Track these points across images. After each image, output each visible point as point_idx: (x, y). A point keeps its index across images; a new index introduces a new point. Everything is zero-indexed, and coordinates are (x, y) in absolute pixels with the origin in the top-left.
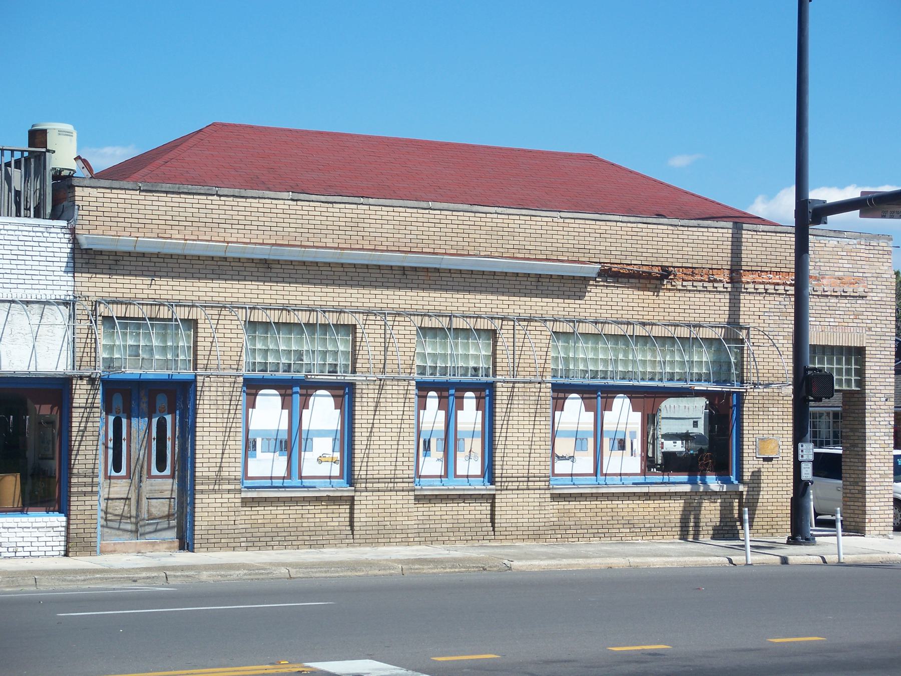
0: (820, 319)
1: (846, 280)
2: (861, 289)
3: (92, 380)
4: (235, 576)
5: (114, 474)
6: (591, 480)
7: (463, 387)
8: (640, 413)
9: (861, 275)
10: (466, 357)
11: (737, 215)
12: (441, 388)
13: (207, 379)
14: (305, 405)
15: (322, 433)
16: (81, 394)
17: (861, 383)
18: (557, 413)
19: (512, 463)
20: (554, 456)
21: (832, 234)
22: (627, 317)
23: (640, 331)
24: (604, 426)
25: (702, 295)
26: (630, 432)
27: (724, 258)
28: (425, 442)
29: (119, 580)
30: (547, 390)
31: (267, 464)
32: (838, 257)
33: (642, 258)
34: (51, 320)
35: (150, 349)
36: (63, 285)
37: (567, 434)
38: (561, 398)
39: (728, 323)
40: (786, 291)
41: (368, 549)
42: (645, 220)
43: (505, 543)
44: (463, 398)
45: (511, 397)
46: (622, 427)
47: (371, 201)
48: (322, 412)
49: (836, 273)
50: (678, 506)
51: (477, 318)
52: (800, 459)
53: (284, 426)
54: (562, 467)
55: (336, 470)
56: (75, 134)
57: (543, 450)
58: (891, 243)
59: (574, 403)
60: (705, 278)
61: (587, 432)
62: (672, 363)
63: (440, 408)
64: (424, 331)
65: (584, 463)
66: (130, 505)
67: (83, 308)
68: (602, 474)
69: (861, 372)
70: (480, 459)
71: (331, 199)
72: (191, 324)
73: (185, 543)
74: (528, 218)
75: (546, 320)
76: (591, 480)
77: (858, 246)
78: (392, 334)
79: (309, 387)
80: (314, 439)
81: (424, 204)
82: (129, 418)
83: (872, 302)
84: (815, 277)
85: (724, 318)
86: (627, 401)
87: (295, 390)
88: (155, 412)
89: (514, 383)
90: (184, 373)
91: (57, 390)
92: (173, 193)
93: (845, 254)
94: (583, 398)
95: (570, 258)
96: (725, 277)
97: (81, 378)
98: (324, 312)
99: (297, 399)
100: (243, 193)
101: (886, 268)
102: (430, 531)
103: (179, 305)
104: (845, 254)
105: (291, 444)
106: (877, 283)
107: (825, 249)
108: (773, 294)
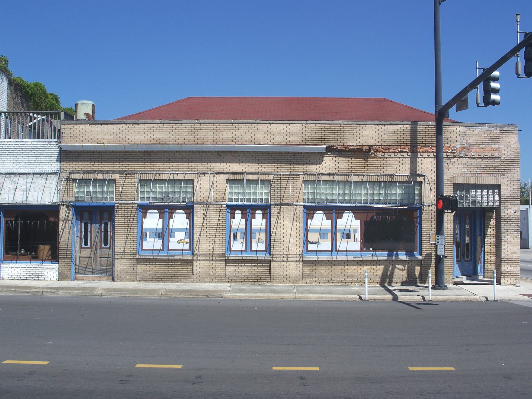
1: (487, 149)
2: (497, 154)
3: (68, 206)
4: (75, 294)
5: (104, 247)
7: (254, 208)
10: (255, 193)
14: (171, 217)
16: (63, 213)
18: (309, 221)
21: (477, 125)
22: (348, 171)
23: (355, 178)
25: (394, 159)
26: (354, 230)
27: (407, 140)
28: (234, 234)
29: (21, 292)
30: (300, 209)
31: (152, 244)
34: (51, 181)
36: (56, 167)
37: (315, 231)
38: (311, 214)
39: (410, 173)
41: (197, 284)
42: (357, 123)
43: (262, 283)
44: (255, 214)
45: (279, 212)
46: (348, 227)
47: (201, 121)
48: (179, 220)
49: (481, 146)
50: (380, 269)
53: (160, 226)
54: (311, 247)
55: (187, 247)
57: (298, 239)
58: (517, 129)
60: (396, 151)
62: (379, 194)
63: (242, 218)
65: (326, 245)
66: (91, 260)
67: (65, 175)
68: (336, 251)
70: (265, 242)
71: (180, 122)
72: (112, 181)
73: (113, 280)
78: (213, 184)
79: (173, 209)
81: (230, 121)
82: (91, 224)
85: (408, 171)
86: (351, 214)
88: (83, 220)
90: (109, 202)
97: (64, 205)
98: (177, 174)
99: (167, 214)
100: (137, 122)
102: (235, 276)
105: (165, 234)
107: (473, 133)
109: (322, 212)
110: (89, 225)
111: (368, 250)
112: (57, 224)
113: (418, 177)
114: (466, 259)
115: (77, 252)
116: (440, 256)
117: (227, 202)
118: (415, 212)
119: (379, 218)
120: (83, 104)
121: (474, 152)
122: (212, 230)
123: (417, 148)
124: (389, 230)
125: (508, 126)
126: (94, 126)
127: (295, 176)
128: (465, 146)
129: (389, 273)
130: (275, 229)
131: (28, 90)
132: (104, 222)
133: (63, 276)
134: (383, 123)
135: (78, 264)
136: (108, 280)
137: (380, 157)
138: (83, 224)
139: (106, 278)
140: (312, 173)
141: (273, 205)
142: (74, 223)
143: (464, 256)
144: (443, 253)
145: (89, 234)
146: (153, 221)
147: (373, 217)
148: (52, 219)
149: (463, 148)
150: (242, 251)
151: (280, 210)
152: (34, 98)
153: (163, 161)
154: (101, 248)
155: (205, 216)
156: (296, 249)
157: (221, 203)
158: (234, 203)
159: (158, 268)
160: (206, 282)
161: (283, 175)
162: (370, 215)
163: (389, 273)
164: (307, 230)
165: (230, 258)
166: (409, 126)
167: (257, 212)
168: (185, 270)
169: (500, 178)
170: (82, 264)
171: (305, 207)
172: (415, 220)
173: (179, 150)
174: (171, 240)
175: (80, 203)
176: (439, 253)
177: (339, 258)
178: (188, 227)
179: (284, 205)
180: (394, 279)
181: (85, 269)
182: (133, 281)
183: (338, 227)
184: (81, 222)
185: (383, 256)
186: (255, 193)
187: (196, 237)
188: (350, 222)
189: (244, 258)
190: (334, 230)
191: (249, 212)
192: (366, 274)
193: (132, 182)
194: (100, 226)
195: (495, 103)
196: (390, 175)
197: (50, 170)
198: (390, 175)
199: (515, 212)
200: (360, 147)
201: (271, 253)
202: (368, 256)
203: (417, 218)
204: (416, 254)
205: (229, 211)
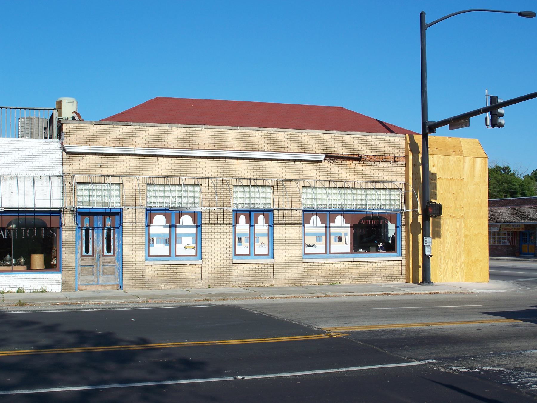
15: (263, 235)
16: (68, 218)
20: (305, 245)
28: (239, 239)
52: (425, 245)
56: (75, 102)
59: (315, 220)
65: (321, 248)
67: (68, 179)
70: (267, 247)
103: (320, 181)
116: (428, 256)
145: (91, 241)
154: (103, 255)
158: (240, 207)
176: (427, 253)
188: (341, 226)
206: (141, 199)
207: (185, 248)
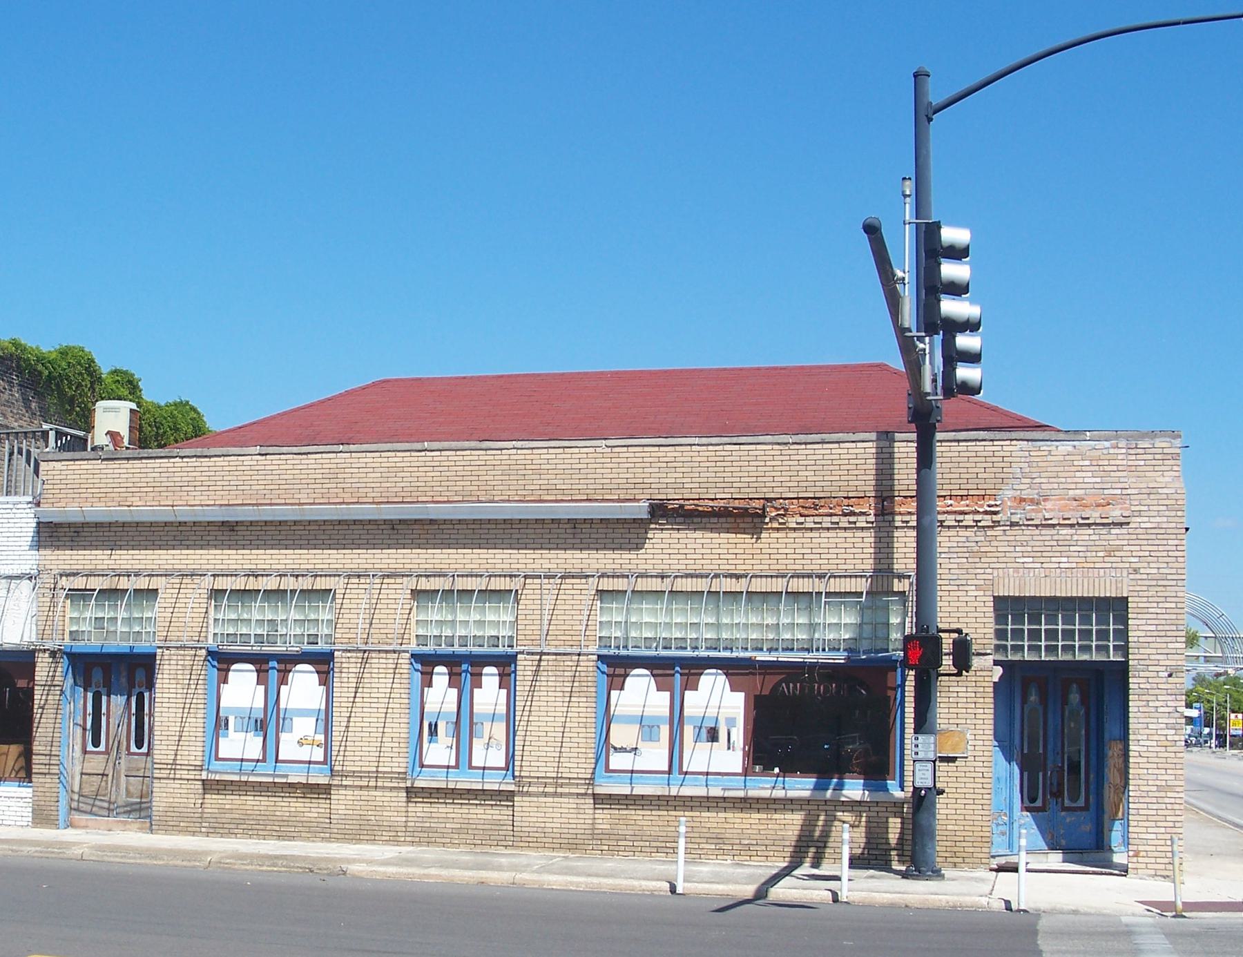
0: (1042, 560)
3: (53, 654)
4: (25, 853)
6: (738, 781)
8: (742, 694)
9: (1119, 492)
11: (997, 421)
12: (453, 662)
13: (167, 652)
14: (283, 681)
17: (1124, 649)
18: (614, 694)
19: (538, 754)
22: (709, 566)
24: (426, 706)
25: (831, 534)
26: (727, 719)
27: (866, 482)
28: (430, 725)
31: (240, 744)
32: (1073, 469)
33: (732, 490)
35: (1052, 634)
36: (28, 560)
37: (628, 719)
39: (875, 570)
40: (977, 521)
42: (735, 440)
44: (481, 674)
45: (536, 672)
46: (712, 712)
47: (352, 448)
48: (303, 687)
49: (1071, 492)
50: (793, 822)
51: (490, 576)
53: (259, 703)
54: (617, 761)
55: (319, 755)
57: (583, 739)
58: (1178, 442)
59: (639, 684)
60: (837, 511)
61: (659, 718)
63: (450, 685)
64: (416, 594)
65: (655, 756)
67: (48, 579)
68: (681, 772)
69: (1123, 634)
73: (152, 831)
74: (561, 450)
75: (587, 576)
76: (738, 781)
77: (1112, 451)
78: (374, 601)
79: (288, 661)
80: (295, 719)
81: (418, 446)
82: (109, 696)
83: (1138, 531)
84: (1032, 500)
85: (869, 565)
87: (273, 665)
89: (542, 654)
90: (143, 646)
91: (23, 661)
92: (135, 459)
93: (1087, 463)
94: (726, 674)
95: (622, 497)
96: (869, 507)
98: (297, 576)
99: (273, 676)
100: (206, 452)
101: (1169, 479)
104: (1087, 463)
105: (268, 723)
106: (1148, 502)
107: (1050, 458)
108: (955, 527)
109: (251, 667)
110: (104, 698)
111: (768, 768)
112: (30, 693)
113: (896, 581)
114: (1067, 803)
115: (76, 762)
117: (413, 646)
118: (890, 674)
119: (795, 687)
120: (106, 410)
121: (1050, 510)
122: (378, 714)
123: (893, 502)
124: (826, 722)
125: (1152, 435)
126: (111, 464)
127: (577, 581)
128: (1025, 495)
129: (817, 834)
130: (526, 713)
131: (40, 367)
132: (137, 690)
133: (42, 817)
134: (802, 438)
135: (76, 789)
136: (141, 829)
137: (795, 529)
138: (90, 695)
139: (137, 825)
140: (618, 572)
141: (522, 653)
142: (68, 693)
143: (1058, 794)
144: (929, 784)
145: (104, 719)
146: (243, 690)
147: (779, 684)
148: (22, 683)
149: (1022, 500)
150: (448, 767)
151: (539, 666)
152: (57, 385)
153: (266, 546)
155: (359, 680)
156: (578, 765)
157: (398, 648)
158: (430, 648)
159: (251, 802)
160: (359, 841)
161: (545, 577)
162: (771, 680)
163: (817, 834)
164: (608, 718)
165: (418, 784)
166: (870, 444)
167: (487, 670)
168: (311, 809)
169: (1125, 580)
170: (86, 791)
171: (601, 658)
172: (890, 693)
173: (298, 518)
174: (283, 736)
175: (80, 646)
177: (687, 791)
178: (323, 707)
179: (548, 654)
180: (828, 850)
181: (92, 803)
182: (194, 833)
183: (687, 712)
184: (86, 690)
185: (801, 786)
186: (480, 624)
187: (338, 730)
188: (719, 700)
189: (451, 786)
190: (677, 718)
191: (466, 671)
192: (682, 829)
193: (195, 595)
194: (128, 700)
195: (969, 389)
196: (820, 577)
197: (16, 570)
198: (820, 577)
199: (1170, 676)
200: (742, 504)
201: (517, 774)
202: (763, 786)
203: (895, 689)
204: (892, 785)
205: (419, 666)
206: (399, 612)
207: (300, 743)
